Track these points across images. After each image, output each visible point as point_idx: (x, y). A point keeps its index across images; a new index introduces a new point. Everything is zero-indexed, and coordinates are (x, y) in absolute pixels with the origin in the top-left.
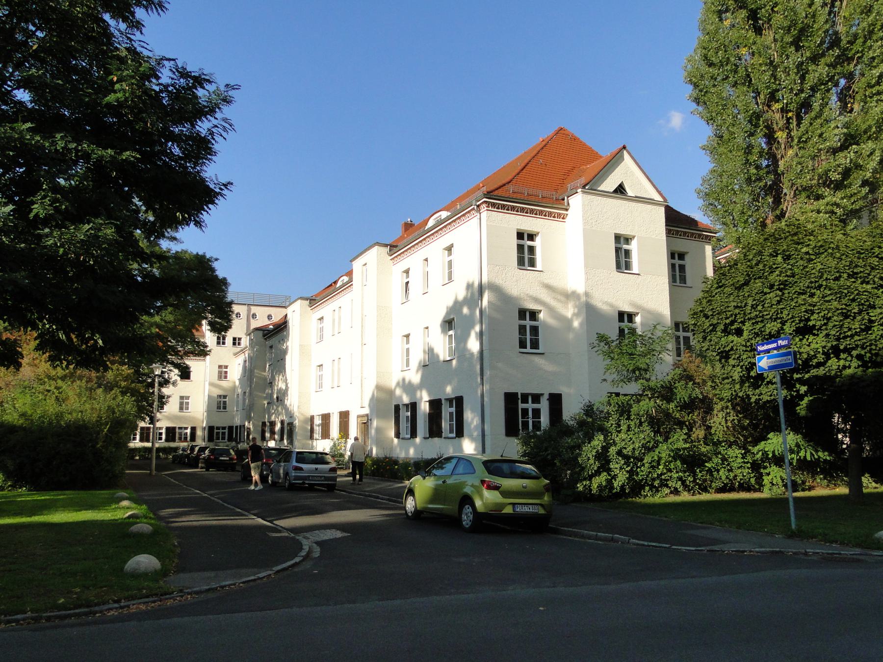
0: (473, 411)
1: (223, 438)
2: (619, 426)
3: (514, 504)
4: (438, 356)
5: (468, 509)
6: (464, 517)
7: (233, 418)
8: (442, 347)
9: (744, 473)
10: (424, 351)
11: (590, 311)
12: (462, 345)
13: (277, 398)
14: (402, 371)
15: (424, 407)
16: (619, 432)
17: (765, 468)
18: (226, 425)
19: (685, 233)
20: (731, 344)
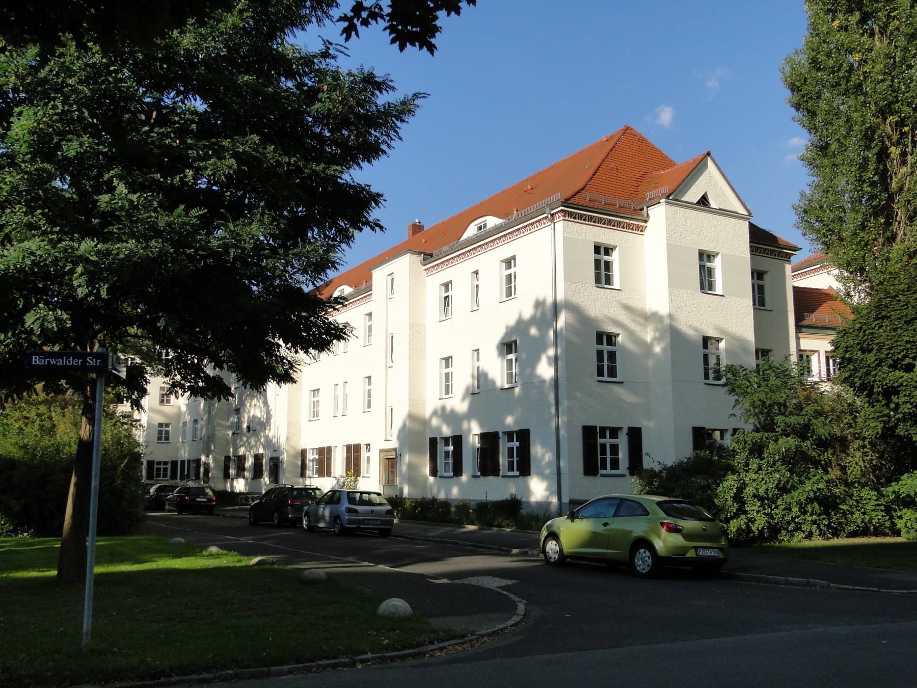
0: (544, 445)
1: (165, 475)
2: (747, 465)
3: (696, 548)
4: (493, 382)
5: (644, 553)
6: (638, 562)
7: (178, 450)
8: (497, 370)
9: (879, 516)
10: (473, 376)
11: (674, 336)
12: (529, 371)
13: (249, 428)
14: (441, 397)
15: (473, 440)
16: (747, 471)
17: (895, 511)
18: (169, 459)
19: (772, 251)
20: (901, 380)
